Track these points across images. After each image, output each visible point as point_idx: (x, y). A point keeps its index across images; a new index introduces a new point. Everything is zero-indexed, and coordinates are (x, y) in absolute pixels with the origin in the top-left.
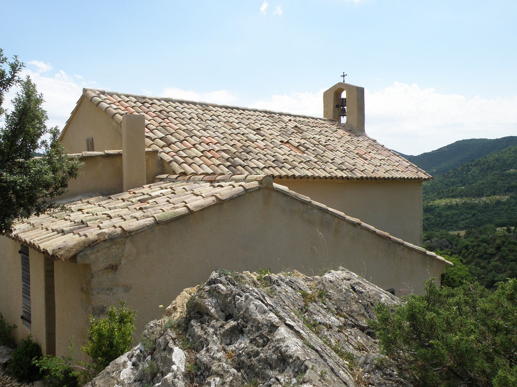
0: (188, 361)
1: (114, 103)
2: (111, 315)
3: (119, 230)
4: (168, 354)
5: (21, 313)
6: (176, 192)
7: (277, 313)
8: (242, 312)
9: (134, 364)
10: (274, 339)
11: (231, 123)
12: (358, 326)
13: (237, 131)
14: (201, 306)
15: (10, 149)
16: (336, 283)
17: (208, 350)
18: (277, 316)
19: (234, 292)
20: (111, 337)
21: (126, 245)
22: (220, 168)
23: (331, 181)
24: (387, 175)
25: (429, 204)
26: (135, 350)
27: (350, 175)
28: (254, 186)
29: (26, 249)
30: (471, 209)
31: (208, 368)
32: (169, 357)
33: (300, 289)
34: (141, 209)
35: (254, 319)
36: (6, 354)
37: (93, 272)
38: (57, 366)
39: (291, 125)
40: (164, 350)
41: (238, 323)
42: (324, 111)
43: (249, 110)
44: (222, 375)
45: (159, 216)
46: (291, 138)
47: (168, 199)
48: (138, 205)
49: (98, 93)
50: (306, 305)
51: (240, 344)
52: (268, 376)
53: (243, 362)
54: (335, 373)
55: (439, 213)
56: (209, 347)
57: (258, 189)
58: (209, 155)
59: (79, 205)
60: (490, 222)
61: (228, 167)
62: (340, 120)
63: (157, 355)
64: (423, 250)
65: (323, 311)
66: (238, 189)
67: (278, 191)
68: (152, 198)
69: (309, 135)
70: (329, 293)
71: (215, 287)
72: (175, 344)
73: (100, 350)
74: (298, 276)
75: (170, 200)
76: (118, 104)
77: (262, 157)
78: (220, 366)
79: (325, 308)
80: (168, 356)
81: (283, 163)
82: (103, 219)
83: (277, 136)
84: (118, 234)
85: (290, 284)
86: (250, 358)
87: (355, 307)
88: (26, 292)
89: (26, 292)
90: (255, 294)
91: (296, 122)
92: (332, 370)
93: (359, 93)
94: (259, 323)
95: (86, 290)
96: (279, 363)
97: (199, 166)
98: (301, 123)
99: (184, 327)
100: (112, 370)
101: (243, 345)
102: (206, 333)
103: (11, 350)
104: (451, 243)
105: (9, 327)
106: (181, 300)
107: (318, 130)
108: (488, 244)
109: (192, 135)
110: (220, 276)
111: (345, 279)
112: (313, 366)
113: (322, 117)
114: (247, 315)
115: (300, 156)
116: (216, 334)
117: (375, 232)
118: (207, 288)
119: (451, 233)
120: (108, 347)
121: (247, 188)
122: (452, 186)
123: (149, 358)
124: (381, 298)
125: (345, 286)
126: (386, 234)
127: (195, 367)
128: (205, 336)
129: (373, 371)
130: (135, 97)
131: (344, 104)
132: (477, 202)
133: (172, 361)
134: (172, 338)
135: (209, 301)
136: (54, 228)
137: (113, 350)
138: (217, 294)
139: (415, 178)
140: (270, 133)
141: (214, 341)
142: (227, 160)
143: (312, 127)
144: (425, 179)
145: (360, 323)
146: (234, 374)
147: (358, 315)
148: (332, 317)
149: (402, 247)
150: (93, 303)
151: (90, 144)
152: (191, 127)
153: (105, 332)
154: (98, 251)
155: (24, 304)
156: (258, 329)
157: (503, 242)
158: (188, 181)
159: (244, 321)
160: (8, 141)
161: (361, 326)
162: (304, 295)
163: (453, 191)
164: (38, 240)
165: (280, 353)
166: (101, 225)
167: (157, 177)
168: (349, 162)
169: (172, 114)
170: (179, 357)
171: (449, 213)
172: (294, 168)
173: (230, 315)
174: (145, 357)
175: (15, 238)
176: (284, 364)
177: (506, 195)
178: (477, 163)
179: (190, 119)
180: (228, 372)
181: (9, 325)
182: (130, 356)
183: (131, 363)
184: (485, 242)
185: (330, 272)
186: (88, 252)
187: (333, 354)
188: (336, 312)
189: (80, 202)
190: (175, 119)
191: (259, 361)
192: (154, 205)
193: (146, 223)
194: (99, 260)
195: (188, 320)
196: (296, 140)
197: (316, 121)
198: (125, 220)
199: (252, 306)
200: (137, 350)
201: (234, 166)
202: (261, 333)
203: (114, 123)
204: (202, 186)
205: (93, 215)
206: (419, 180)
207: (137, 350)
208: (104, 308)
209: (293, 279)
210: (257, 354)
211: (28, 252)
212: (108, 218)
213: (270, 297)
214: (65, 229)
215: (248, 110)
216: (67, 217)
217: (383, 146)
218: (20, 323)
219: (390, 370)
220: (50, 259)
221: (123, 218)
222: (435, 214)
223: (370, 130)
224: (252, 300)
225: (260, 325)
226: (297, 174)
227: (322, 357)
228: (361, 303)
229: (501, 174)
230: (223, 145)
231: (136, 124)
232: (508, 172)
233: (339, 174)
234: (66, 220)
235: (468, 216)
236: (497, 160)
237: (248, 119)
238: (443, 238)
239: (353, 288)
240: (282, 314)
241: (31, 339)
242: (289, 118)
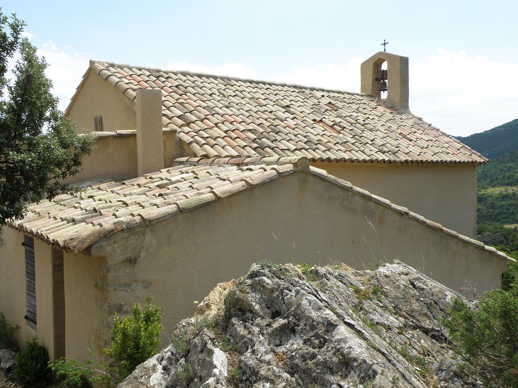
0: (231, 364)
1: (125, 77)
2: (136, 313)
3: (138, 219)
4: (207, 356)
5: (25, 313)
6: (199, 176)
7: (333, 310)
8: (292, 309)
9: (164, 368)
10: (334, 340)
11: (257, 99)
12: (420, 328)
13: (264, 108)
14: (243, 302)
15: (17, 124)
16: (392, 277)
17: (253, 352)
18: (335, 313)
19: (282, 286)
20: (137, 337)
21: (146, 236)
22: (246, 150)
23: (372, 164)
24: (435, 159)
25: (480, 193)
26: (165, 352)
28: (289, 170)
29: (30, 240)
31: (255, 373)
32: (209, 359)
33: (352, 284)
34: (161, 195)
35: (308, 317)
36: (8, 359)
37: (109, 266)
38: (75, 371)
39: (325, 101)
40: (202, 351)
41: (289, 321)
42: (362, 86)
44: (273, 380)
45: (182, 202)
46: (325, 116)
47: (191, 184)
48: (157, 191)
49: (107, 65)
50: (360, 302)
51: (292, 345)
52: (328, 381)
53: (297, 365)
54: (407, 380)
55: (491, 204)
56: (255, 348)
57: (293, 173)
58: (234, 135)
59: (89, 191)
61: (255, 149)
62: (379, 95)
63: (193, 357)
64: (481, 244)
65: (380, 310)
66: (270, 173)
68: (172, 183)
69: (345, 113)
70: (384, 289)
71: (259, 281)
72: (214, 345)
73: (125, 352)
74: (346, 269)
75: (193, 185)
76: (130, 78)
77: (293, 137)
78: (269, 369)
79: (381, 307)
80: (206, 358)
81: (316, 145)
82: (119, 206)
83: (308, 114)
84: (137, 223)
85: (340, 278)
86: (305, 360)
87: (416, 306)
88: (31, 289)
89: (31, 289)
90: (306, 288)
91: (330, 97)
92: (403, 376)
93: (403, 63)
94: (313, 321)
95: (101, 286)
96: (340, 367)
97: (223, 148)
99: (223, 326)
100: (140, 374)
101: (295, 346)
102: (250, 333)
103: (14, 354)
104: (507, 239)
105: (10, 328)
106: (216, 298)
107: (355, 107)
109: (214, 112)
110: (263, 269)
111: (402, 273)
112: (383, 371)
113: (359, 92)
114: (299, 312)
115: (336, 137)
116: (262, 334)
117: (425, 222)
118: (249, 282)
119: (507, 226)
120: (133, 348)
121: (281, 171)
122: (508, 171)
123: (182, 361)
124: (446, 295)
125: (403, 281)
126: (438, 225)
127: (240, 371)
128: (249, 336)
129: (450, 378)
130: (149, 70)
131: (385, 77)
133: (213, 364)
134: (211, 339)
135: (253, 297)
136: (63, 217)
137: (139, 353)
138: (262, 289)
139: (468, 161)
141: (260, 342)
142: (254, 141)
143: (348, 104)
144: (480, 163)
145: (423, 324)
146: (287, 380)
147: (420, 314)
148: (390, 317)
149: (456, 240)
150: (109, 301)
151: (98, 122)
152: (212, 104)
153: (130, 331)
154: (114, 243)
155: (28, 302)
156: (313, 327)
158: (212, 164)
159: (296, 319)
160: (14, 115)
161: (424, 328)
162: (357, 291)
163: (509, 178)
164: (46, 231)
165: (342, 356)
166: (116, 213)
167: (175, 160)
168: (391, 143)
169: (190, 89)
170: (220, 358)
171: (503, 203)
172: (329, 150)
173: (277, 312)
174: (177, 360)
175: (19, 228)
176: (347, 369)
179: (211, 95)
180: (280, 377)
181: (11, 326)
182: (160, 359)
183: (161, 367)
185: (384, 266)
186: (104, 243)
187: (401, 358)
188: (394, 312)
189: (89, 188)
190: (194, 95)
191: (317, 364)
192: (175, 191)
193: (168, 210)
194: (116, 252)
195: (228, 318)
196: (330, 118)
197: (353, 97)
198: (143, 207)
199: (304, 302)
200: (167, 352)
201: (262, 147)
202: (316, 333)
203: (126, 100)
204: (228, 170)
205: (106, 202)
206: (473, 164)
207: (167, 352)
208: (121, 306)
209: (343, 272)
210: (313, 356)
211: (33, 244)
212: (124, 205)
213: (323, 292)
214: (76, 218)
215: (275, 85)
216: (76, 205)
217: (430, 125)
218: (24, 324)
219: (473, 378)
220: (58, 251)
221: (141, 206)
222: (488, 204)
223: (415, 106)
224: (304, 294)
225: (315, 323)
226: (333, 157)
227: (390, 361)
228: (422, 301)
230: (248, 124)
231: (151, 100)
233: (381, 157)
234: (76, 208)
237: (275, 95)
238: (497, 232)
239: (412, 284)
240: (339, 311)
241: (37, 341)
242: (322, 93)
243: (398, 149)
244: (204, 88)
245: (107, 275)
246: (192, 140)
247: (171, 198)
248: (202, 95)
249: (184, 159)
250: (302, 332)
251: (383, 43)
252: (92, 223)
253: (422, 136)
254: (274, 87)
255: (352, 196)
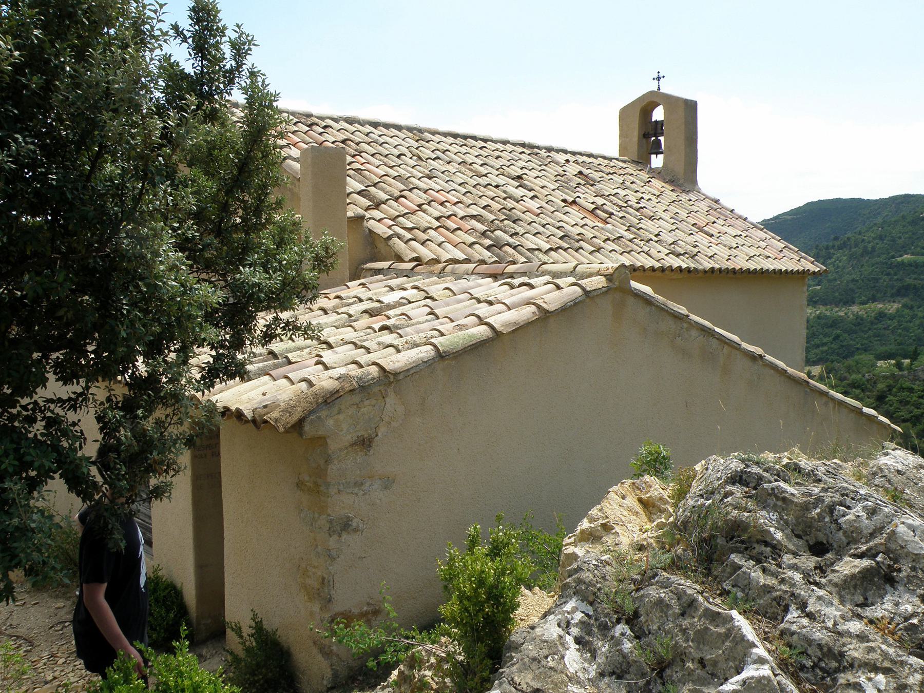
9: (578, 641)
11: (471, 164)
13: (484, 181)
21: (388, 400)
24: (752, 265)
27: (692, 266)
30: (831, 326)
35: (916, 555)
37: (330, 452)
39: (572, 169)
43: (495, 142)
58: (451, 224)
60: (865, 350)
61: (488, 248)
66: (570, 291)
67: (638, 295)
69: (607, 189)
71: (773, 489)
77: (541, 229)
81: (578, 241)
84: (373, 379)
91: (578, 163)
97: (439, 245)
98: (589, 166)
108: (863, 390)
113: (617, 155)
121: (588, 289)
131: (660, 131)
132: (842, 314)
138: (779, 503)
140: (541, 185)
142: (484, 234)
149: (824, 399)
150: (329, 511)
157: (890, 388)
158: (441, 274)
168: (685, 241)
169: (364, 146)
177: (894, 302)
178: (844, 243)
179: (399, 157)
180: (903, 663)
182: (563, 624)
184: (857, 387)
186: (323, 413)
190: (372, 155)
193: (421, 355)
194: (340, 428)
196: (587, 198)
197: (612, 164)
201: (497, 245)
206: (804, 273)
215: (492, 141)
217: (732, 211)
223: (708, 177)
229: (886, 263)
232: (899, 259)
233: (675, 262)
235: (825, 340)
236: (881, 238)
241: (160, 573)
243: (696, 250)
244: (385, 145)
245: (326, 470)
246: (391, 232)
247: (411, 334)
248: (386, 156)
249: (384, 265)
250: (909, 582)
251: (656, 76)
252: (286, 377)
253: (725, 229)
254: (490, 145)
255: (688, 329)
